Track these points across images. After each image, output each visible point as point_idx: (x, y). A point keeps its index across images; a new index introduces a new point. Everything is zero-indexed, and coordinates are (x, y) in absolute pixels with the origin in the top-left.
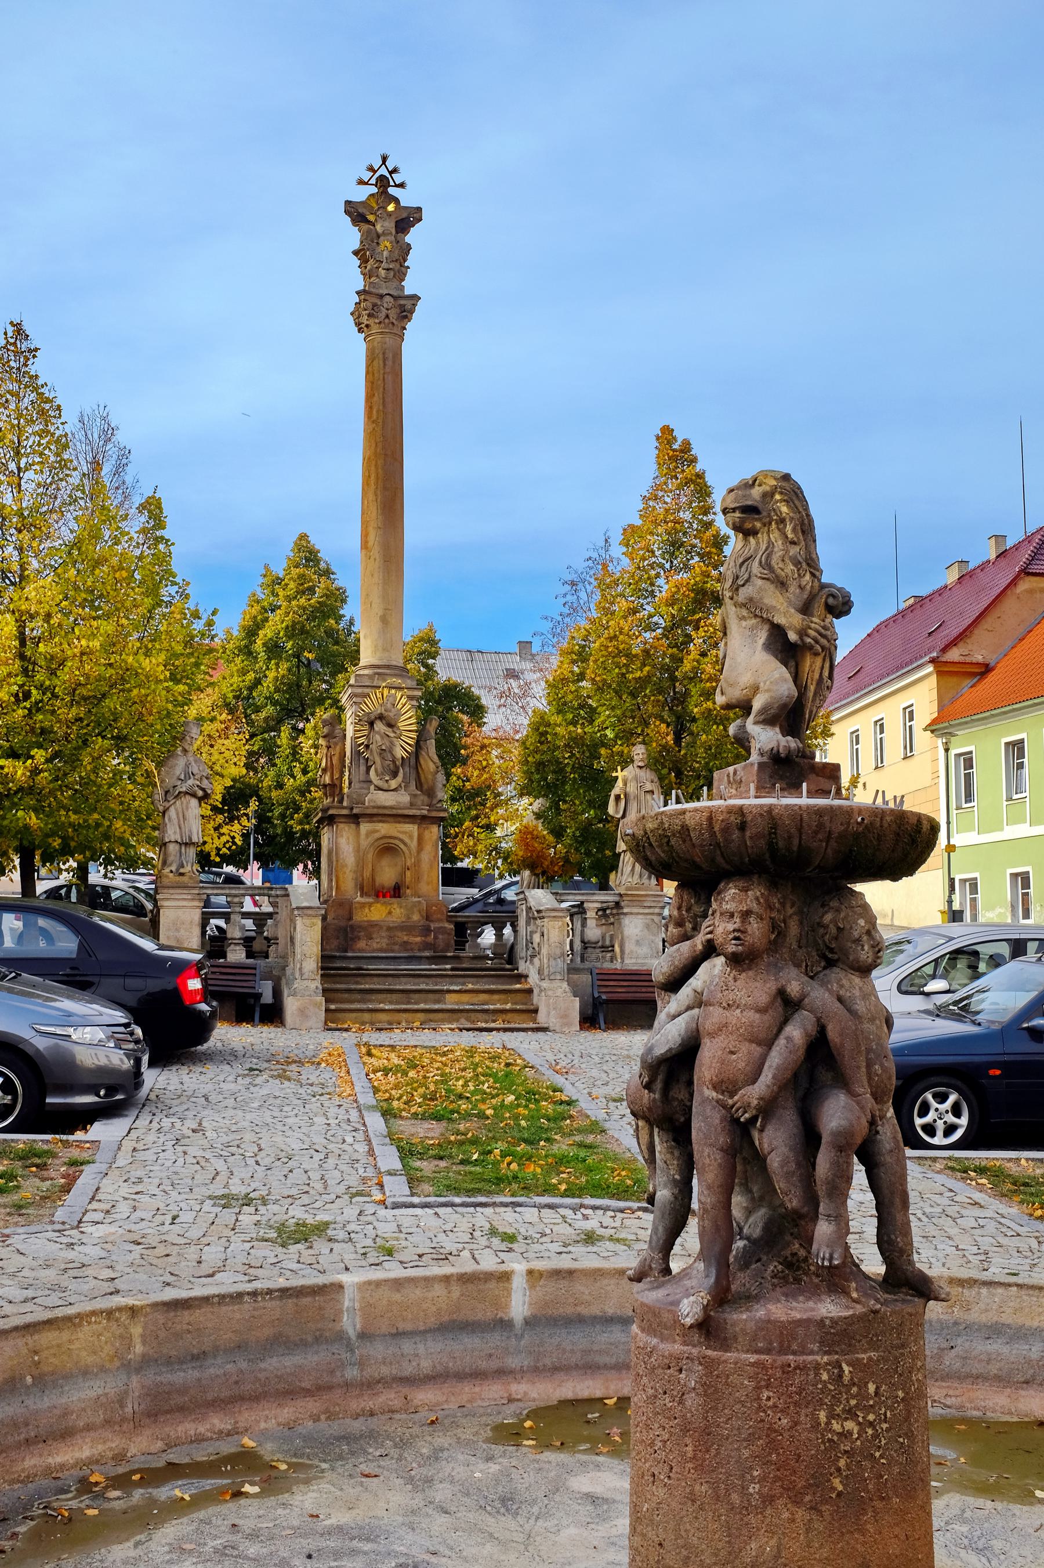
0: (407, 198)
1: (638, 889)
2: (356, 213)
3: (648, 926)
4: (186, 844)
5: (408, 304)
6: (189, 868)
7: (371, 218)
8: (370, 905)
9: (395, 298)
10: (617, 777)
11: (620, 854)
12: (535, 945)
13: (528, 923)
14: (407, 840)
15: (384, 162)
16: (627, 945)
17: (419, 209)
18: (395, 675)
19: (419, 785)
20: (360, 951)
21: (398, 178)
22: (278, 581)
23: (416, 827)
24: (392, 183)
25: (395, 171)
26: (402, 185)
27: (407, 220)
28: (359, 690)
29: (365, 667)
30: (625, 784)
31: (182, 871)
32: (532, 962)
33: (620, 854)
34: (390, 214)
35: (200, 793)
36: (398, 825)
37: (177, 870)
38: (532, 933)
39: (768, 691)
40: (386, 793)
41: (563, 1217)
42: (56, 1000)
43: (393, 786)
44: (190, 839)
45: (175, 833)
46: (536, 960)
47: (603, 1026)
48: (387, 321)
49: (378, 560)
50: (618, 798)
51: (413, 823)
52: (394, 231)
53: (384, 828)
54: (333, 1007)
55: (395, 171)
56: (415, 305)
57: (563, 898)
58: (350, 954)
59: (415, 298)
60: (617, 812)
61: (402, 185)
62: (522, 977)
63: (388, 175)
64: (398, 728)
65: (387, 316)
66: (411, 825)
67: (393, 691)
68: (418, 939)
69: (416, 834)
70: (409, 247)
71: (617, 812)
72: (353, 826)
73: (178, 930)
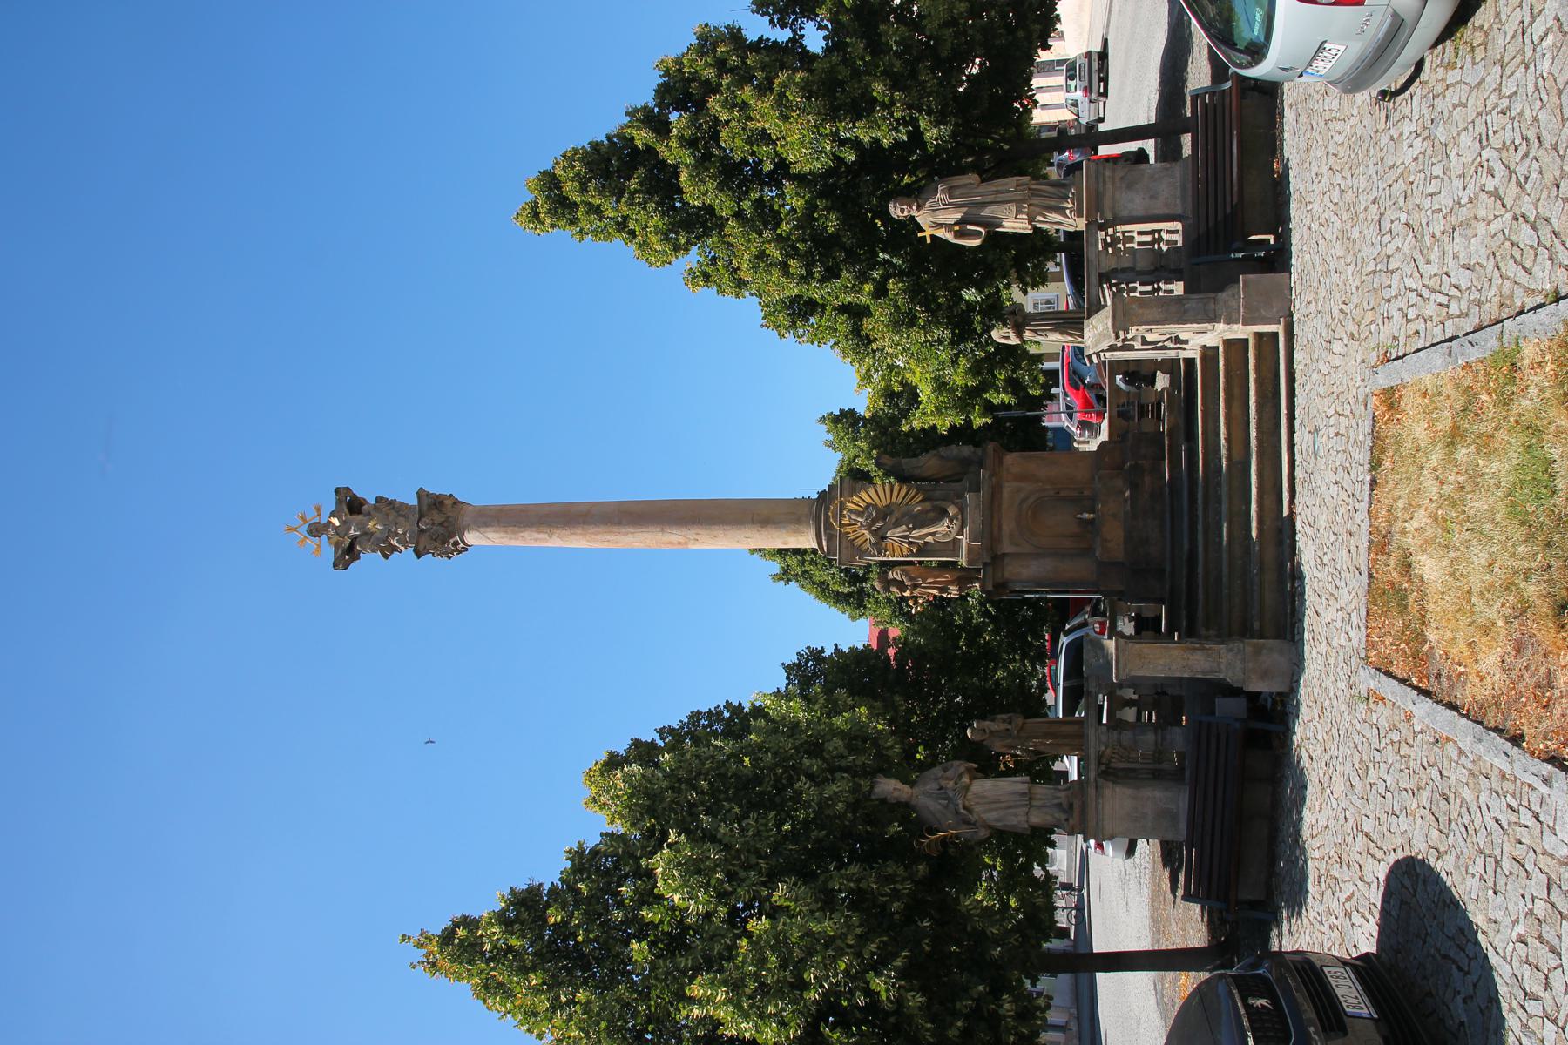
0: (330, 503)
2: (347, 554)
5: (426, 501)
6: (1062, 794)
7: (347, 542)
9: (421, 516)
10: (932, 236)
11: (1035, 228)
13: (1131, 348)
14: (1022, 495)
16: (1156, 212)
17: (337, 491)
18: (827, 509)
22: (785, 572)
25: (304, 519)
26: (318, 509)
27: (352, 505)
29: (820, 544)
30: (940, 225)
31: (1065, 806)
32: (1186, 342)
33: (1035, 228)
34: (343, 523)
37: (1064, 811)
38: (1144, 342)
39: (1434, 442)
44: (1024, 794)
45: (1016, 815)
46: (1183, 337)
50: (961, 234)
55: (304, 519)
56: (428, 494)
58: (1168, 568)
59: (421, 494)
60: (977, 234)
61: (318, 509)
62: (1209, 354)
64: (888, 506)
68: (1147, 479)
70: (379, 499)
71: (977, 234)
72: (1006, 560)
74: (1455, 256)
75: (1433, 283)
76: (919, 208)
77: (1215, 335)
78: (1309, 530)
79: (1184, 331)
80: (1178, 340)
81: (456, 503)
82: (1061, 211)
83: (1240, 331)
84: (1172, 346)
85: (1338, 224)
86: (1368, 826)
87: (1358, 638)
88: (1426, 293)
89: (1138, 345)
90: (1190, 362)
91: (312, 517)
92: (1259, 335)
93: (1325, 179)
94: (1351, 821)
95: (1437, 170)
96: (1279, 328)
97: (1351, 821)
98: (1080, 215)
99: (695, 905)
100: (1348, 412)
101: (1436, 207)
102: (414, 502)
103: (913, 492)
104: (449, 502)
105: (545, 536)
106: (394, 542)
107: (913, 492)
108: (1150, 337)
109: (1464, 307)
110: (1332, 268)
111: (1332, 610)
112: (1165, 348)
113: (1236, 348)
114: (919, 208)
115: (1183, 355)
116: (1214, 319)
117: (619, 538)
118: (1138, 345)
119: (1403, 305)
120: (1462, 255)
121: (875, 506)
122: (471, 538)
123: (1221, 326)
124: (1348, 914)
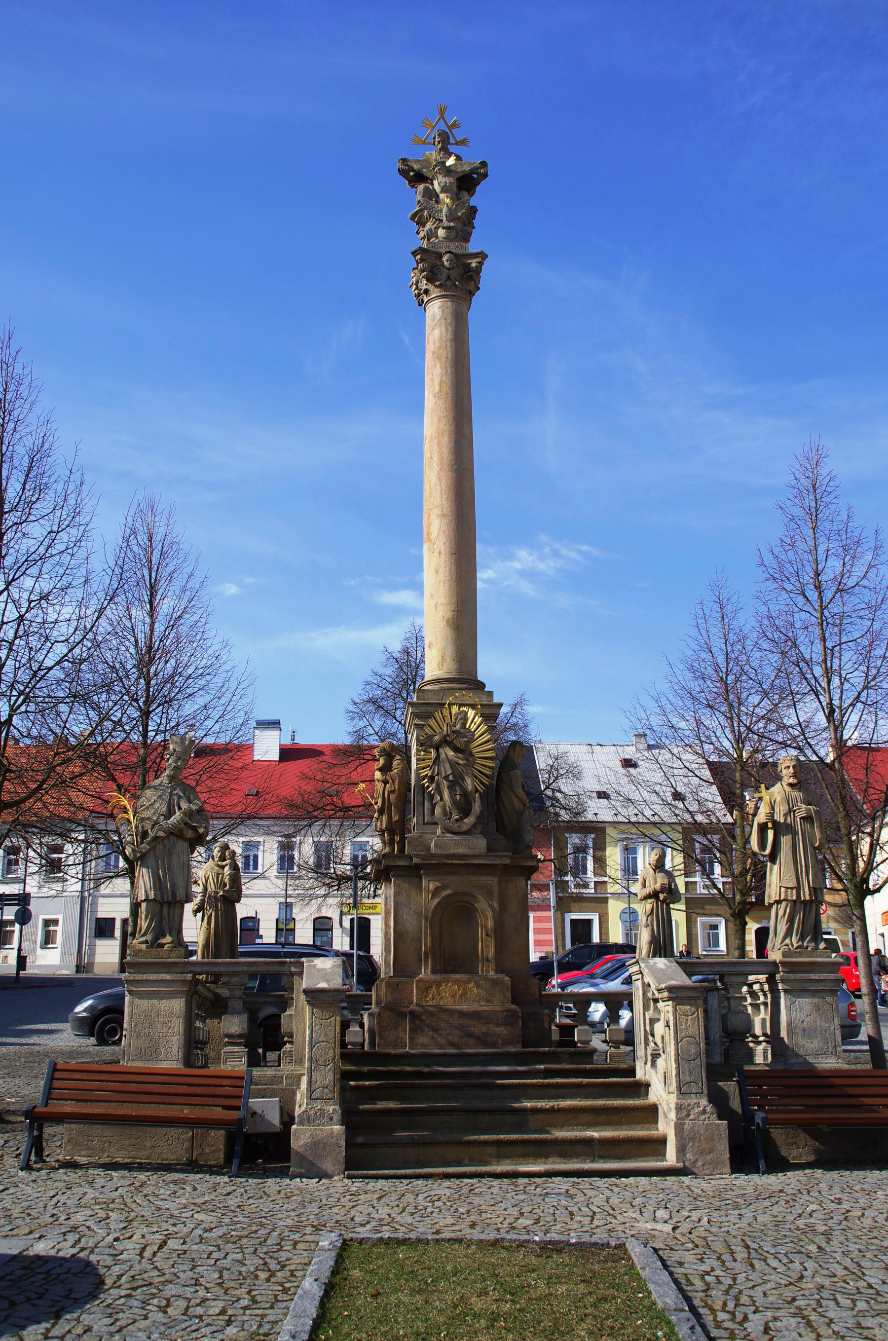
1: (800, 955)
3: (817, 1008)
4: (169, 903)
8: (438, 984)
11: (771, 905)
12: (658, 1040)
13: (646, 1008)
15: (442, 117)
19: (501, 828)
20: (423, 1046)
21: (458, 134)
23: (496, 879)
24: (452, 141)
25: (454, 125)
26: (463, 142)
28: (423, 709)
29: (430, 682)
32: (654, 1065)
35: (190, 834)
36: (473, 878)
38: (653, 1021)
40: (456, 838)
41: (757, 675)
42: (797, 935)
43: (465, 828)
44: (174, 895)
46: (660, 1062)
47: (762, 1165)
48: (449, 283)
49: (443, 553)
51: (493, 875)
52: (455, 189)
53: (457, 883)
54: (360, 1139)
56: (481, 264)
57: (694, 969)
60: (762, 846)
61: (463, 142)
62: (643, 1088)
63: (447, 130)
64: (471, 754)
65: (449, 278)
66: (490, 878)
67: (465, 709)
69: (496, 889)
70: (473, 211)
73: (151, 1025)
74: (775, 1319)
75: (744, 1299)
76: (790, 785)
77: (662, 1093)
78: (465, 1190)
79: (667, 1063)
80: (655, 1056)
81: (471, 294)
82: (788, 933)
83: (666, 1126)
84: (649, 1052)
85: (790, 1218)
86: (171, 1244)
87: (364, 1232)
88: (733, 1292)
89: (650, 1014)
90: (632, 1072)
91: (458, 134)
92: (663, 1141)
93: (834, 1206)
94: (172, 1229)
95: (861, 1305)
96: (671, 1158)
97: (172, 1229)
98: (784, 955)
99: (453, 158)
100: (596, 1222)
101: (824, 1302)
102: (473, 247)
103: (485, 781)
104: (471, 286)
105: (437, 389)
106: (429, 226)
107: (485, 781)
108: (659, 1028)
109: (727, 1324)
110: (743, 1211)
111: (387, 1210)
112: (647, 1044)
113: (651, 1113)
114: (790, 785)
115: (639, 1065)
116: (681, 1091)
117: (436, 468)
118: (650, 1014)
119: (718, 1272)
120: (779, 1324)
121: (472, 740)
122: (436, 308)
123: (673, 1099)
124: (74, 1229)
